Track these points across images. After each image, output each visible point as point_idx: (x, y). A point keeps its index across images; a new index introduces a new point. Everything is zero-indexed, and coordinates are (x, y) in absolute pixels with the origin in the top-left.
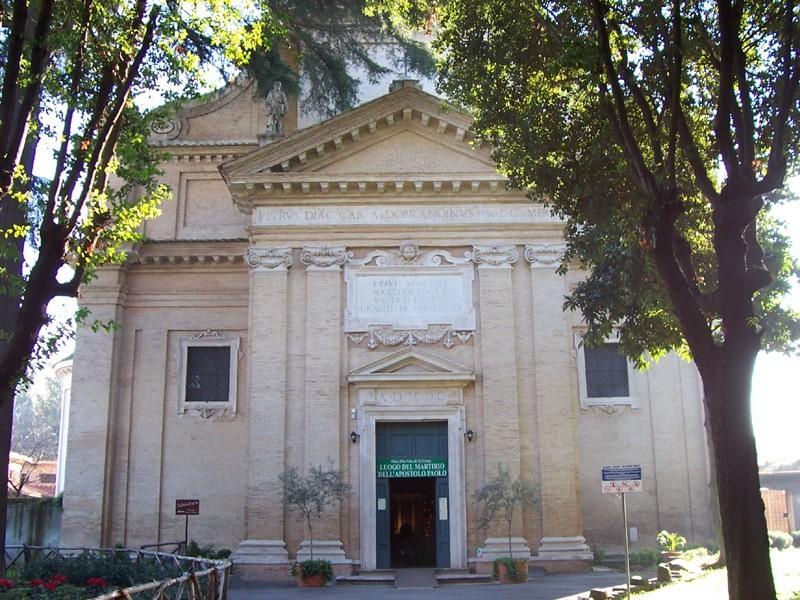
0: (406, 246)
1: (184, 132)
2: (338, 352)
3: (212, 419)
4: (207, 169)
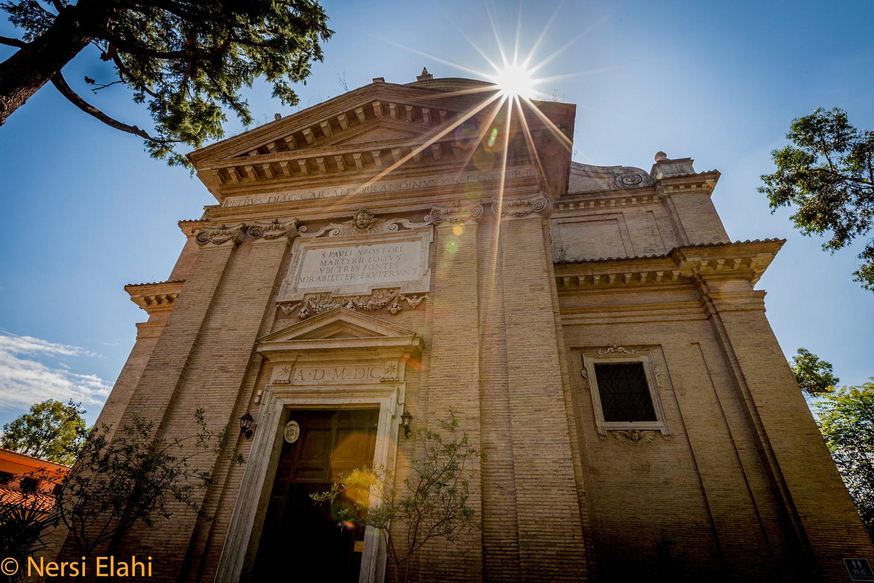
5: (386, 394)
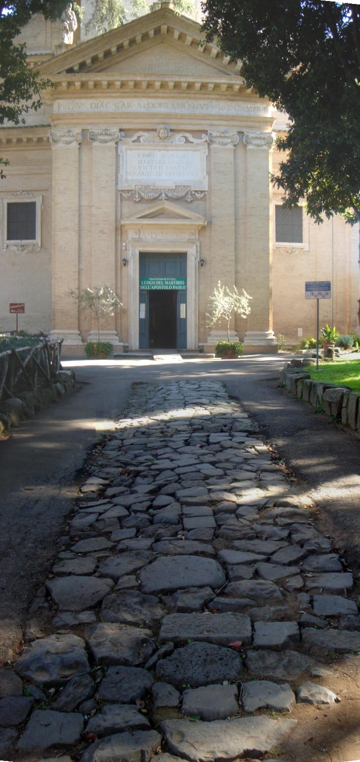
3: (25, 251)
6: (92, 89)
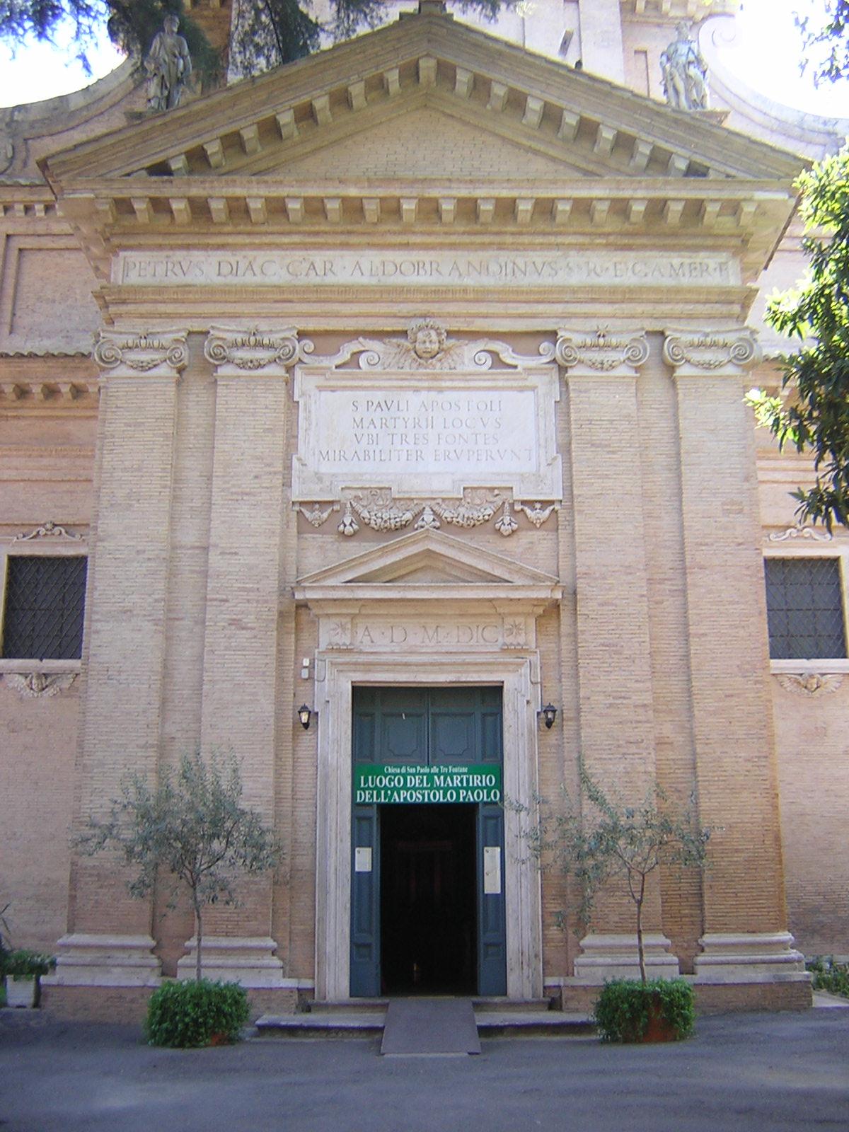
0: (420, 329)
1: (18, 163)
2: (277, 540)
3: (50, 691)
4: (56, 228)
5: (511, 668)
6: (222, 224)
